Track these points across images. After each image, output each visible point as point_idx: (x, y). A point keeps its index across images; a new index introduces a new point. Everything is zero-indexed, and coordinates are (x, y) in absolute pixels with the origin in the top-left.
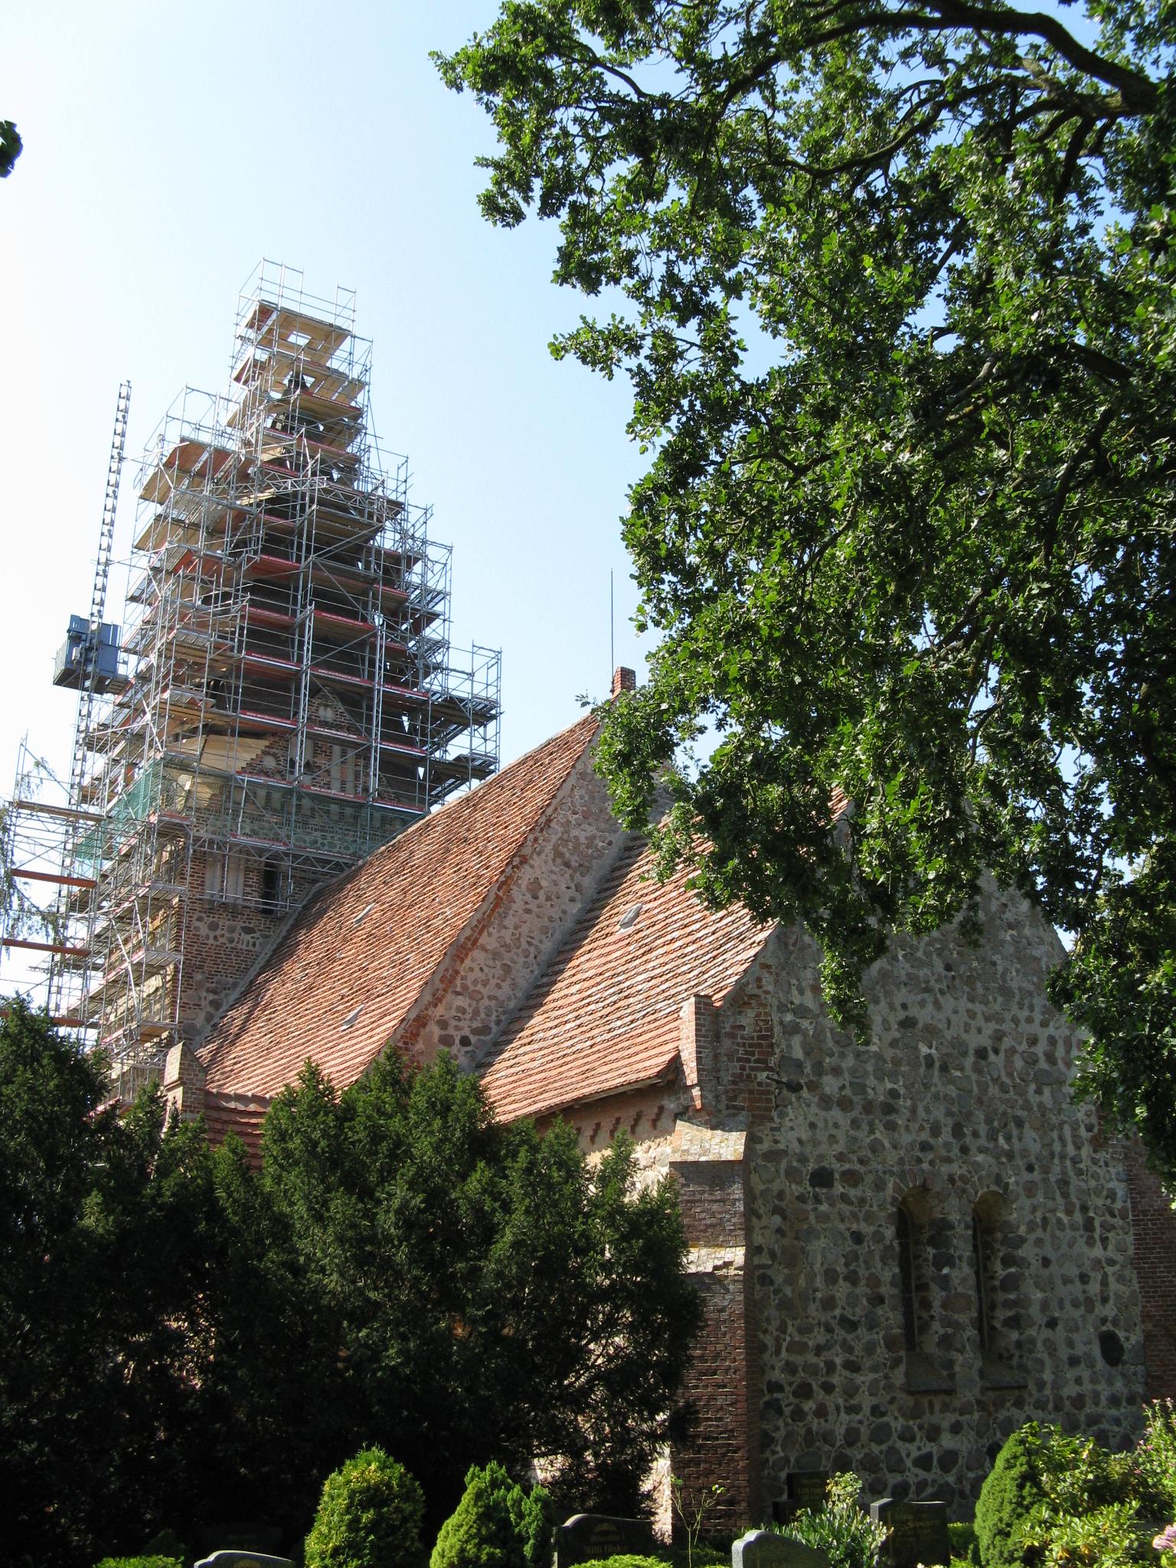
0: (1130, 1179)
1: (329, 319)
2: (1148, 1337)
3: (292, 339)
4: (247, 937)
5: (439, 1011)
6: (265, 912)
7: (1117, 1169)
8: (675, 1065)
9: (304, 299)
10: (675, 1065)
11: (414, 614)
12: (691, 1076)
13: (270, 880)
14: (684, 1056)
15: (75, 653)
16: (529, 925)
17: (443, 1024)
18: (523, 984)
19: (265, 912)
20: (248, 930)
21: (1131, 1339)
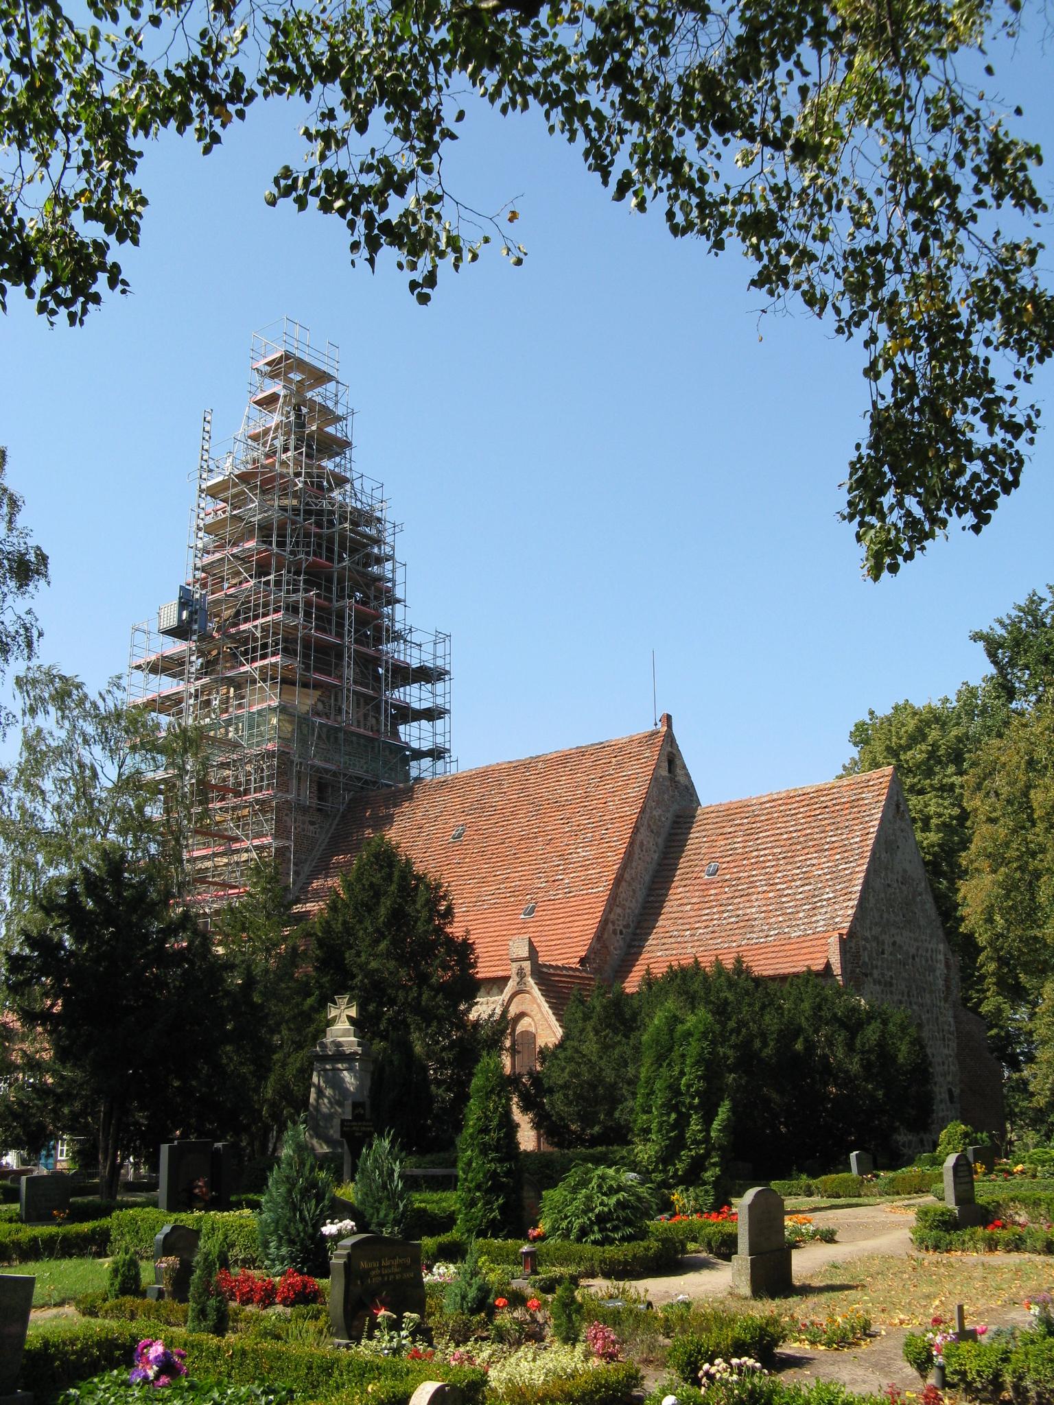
0: (955, 1017)
1: (324, 368)
2: (962, 1091)
3: (291, 376)
4: (311, 828)
5: (612, 916)
6: (319, 810)
7: (951, 1013)
8: (828, 966)
9: (301, 346)
10: (828, 966)
11: (380, 594)
12: (837, 969)
13: (322, 788)
14: (832, 961)
15: (185, 614)
16: (644, 868)
17: (613, 923)
18: (640, 900)
19: (319, 810)
20: (312, 823)
21: (956, 1091)
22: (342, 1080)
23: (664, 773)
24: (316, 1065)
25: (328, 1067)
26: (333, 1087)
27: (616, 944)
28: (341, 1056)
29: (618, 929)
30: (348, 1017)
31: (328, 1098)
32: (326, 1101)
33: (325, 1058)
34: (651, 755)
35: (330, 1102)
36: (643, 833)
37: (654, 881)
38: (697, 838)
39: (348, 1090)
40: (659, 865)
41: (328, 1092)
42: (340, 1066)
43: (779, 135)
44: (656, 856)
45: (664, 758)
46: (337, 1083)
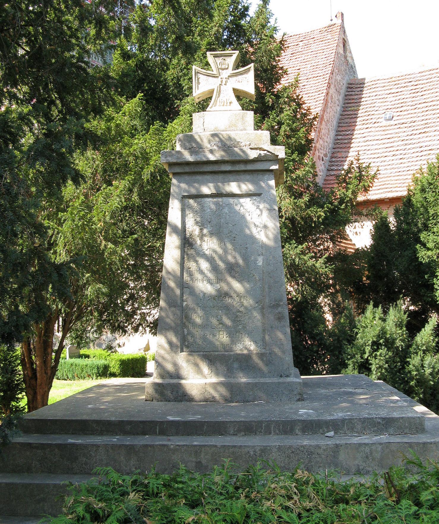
18: (332, 138)
22: (240, 222)
23: (341, 51)
24: (177, 186)
25: (206, 190)
26: (217, 232)
27: (320, 168)
28: (234, 165)
29: (322, 155)
30: (239, 95)
31: (210, 260)
32: (205, 265)
33: (199, 169)
34: (334, 39)
35: (215, 268)
36: (332, 91)
37: (340, 124)
38: (368, 97)
39: (252, 238)
40: (341, 115)
41: (210, 245)
42: (233, 187)
43: (142, 94)
44: (339, 108)
45: (341, 41)
46: (226, 227)
